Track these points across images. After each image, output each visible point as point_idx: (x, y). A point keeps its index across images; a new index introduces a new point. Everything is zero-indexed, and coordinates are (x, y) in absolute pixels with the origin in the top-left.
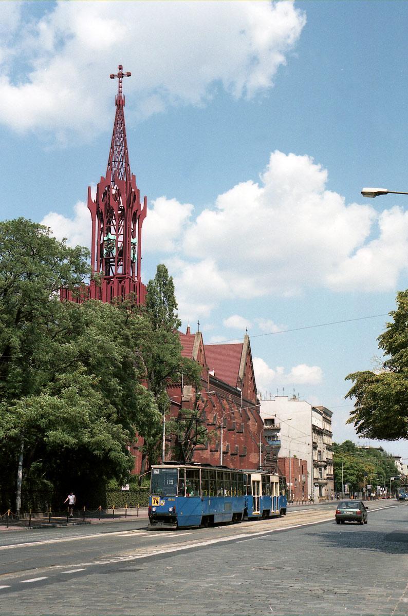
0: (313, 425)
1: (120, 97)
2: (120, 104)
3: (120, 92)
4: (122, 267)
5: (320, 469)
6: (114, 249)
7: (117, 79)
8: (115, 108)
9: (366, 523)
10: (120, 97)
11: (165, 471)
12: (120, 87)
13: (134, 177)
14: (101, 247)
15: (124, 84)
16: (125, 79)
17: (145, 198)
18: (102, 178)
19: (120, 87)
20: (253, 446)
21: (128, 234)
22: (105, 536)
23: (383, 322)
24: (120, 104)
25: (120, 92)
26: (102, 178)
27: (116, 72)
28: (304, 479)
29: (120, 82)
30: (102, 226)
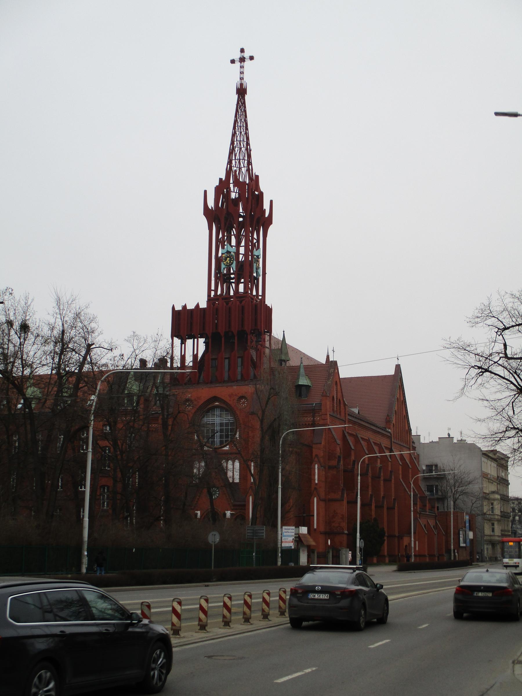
0: (448, 433)
1: (241, 85)
2: (241, 92)
3: (242, 79)
4: (243, 284)
5: (493, 524)
6: (233, 263)
7: (238, 64)
8: (236, 97)
9: (519, 563)
10: (241, 85)
11: (42, 573)
12: (242, 73)
13: (257, 177)
14: (219, 261)
15: (245, 70)
16: (247, 63)
17: (271, 202)
18: (221, 180)
19: (242, 73)
20: (92, 412)
21: (251, 246)
22: (451, 525)
23: (454, 618)
24: (241, 92)
25: (242, 79)
26: (221, 180)
27: (237, 56)
28: (422, 522)
29: (242, 67)
30: (221, 236)
